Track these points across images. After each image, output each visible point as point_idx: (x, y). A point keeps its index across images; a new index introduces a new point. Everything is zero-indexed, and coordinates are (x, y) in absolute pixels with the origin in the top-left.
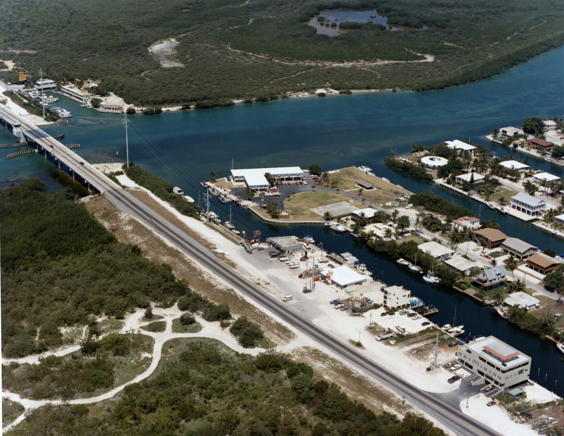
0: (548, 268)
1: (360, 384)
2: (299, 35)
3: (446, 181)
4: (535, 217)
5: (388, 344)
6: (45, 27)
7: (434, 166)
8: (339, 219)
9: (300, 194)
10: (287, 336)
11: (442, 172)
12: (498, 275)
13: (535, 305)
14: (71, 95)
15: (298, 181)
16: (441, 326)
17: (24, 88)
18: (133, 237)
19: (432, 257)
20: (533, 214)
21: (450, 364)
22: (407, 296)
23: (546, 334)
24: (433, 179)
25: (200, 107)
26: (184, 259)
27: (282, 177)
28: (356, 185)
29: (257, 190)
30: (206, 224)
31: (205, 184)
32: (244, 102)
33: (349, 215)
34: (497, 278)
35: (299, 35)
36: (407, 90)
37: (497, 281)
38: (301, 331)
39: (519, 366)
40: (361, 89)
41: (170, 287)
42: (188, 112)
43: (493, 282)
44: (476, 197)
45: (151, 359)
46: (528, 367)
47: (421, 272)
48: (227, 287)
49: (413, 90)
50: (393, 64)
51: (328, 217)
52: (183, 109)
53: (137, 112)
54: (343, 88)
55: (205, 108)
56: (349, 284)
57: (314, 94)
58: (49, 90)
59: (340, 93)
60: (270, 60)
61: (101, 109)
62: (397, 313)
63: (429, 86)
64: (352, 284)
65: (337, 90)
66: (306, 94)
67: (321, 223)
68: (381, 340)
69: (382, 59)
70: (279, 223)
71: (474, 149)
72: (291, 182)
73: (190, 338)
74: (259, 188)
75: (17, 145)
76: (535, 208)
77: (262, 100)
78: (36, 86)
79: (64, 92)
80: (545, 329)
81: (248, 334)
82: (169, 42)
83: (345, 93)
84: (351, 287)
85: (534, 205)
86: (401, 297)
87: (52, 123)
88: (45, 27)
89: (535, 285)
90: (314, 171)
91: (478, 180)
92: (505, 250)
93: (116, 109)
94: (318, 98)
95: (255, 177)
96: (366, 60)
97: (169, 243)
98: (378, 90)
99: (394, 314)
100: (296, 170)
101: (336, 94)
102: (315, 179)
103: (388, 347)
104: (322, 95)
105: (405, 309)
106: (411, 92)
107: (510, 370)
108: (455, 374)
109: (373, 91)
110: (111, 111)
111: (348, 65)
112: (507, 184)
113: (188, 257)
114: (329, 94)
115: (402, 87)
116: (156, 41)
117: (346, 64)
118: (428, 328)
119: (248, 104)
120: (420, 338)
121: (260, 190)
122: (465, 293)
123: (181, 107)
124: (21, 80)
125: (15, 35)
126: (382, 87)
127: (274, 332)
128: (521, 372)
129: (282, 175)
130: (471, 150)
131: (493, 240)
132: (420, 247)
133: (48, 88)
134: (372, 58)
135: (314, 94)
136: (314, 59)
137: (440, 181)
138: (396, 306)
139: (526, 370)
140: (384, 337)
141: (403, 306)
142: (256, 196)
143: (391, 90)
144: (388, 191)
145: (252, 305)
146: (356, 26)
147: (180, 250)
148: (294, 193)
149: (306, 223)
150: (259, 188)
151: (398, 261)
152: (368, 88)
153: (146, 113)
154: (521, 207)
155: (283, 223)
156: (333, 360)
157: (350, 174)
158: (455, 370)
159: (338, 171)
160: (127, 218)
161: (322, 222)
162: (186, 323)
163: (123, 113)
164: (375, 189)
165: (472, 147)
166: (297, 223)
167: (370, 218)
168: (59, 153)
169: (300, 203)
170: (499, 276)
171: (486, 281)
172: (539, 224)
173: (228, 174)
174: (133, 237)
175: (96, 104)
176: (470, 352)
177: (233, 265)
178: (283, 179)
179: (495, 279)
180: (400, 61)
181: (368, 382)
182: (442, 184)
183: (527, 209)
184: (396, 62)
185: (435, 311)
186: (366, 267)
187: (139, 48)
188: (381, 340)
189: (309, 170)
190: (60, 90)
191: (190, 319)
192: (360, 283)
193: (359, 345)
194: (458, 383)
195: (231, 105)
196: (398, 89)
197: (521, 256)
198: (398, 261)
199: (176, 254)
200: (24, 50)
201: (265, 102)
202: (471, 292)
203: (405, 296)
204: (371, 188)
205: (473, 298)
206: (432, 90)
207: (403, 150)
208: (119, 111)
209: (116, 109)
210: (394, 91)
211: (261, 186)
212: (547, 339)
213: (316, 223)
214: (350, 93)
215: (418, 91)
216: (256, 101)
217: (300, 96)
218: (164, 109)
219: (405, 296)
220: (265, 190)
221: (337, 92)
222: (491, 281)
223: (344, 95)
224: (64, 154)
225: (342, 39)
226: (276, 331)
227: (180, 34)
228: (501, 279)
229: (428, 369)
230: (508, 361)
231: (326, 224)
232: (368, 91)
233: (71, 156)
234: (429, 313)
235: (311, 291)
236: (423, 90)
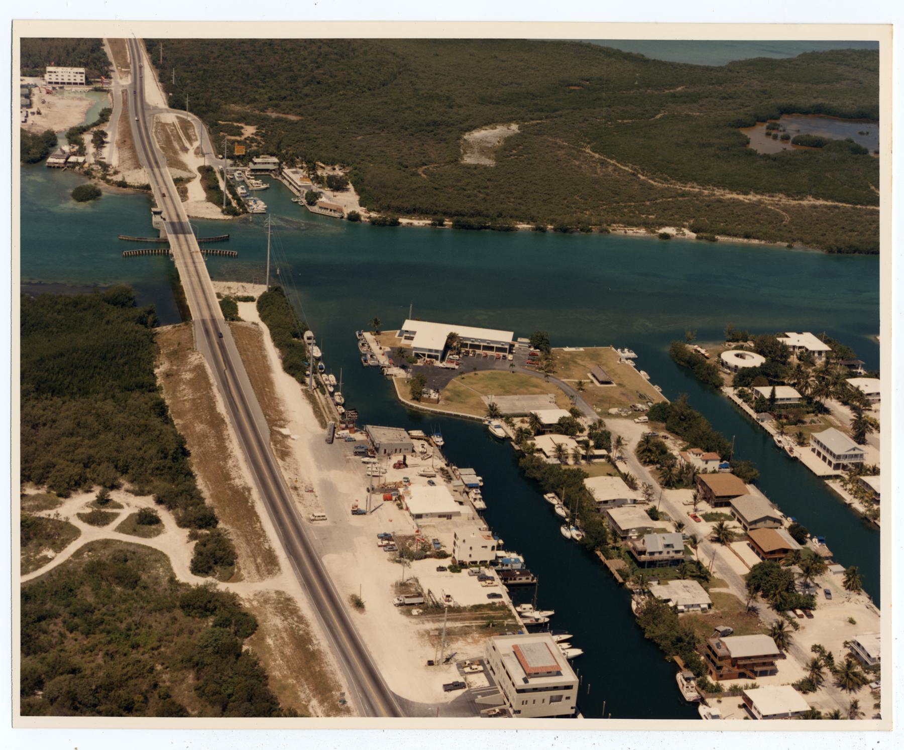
0: (773, 552)
1: (307, 662)
2: (710, 145)
3: (736, 392)
4: (839, 472)
5: (409, 613)
6: (340, 86)
7: (736, 366)
8: (508, 419)
9: (487, 372)
10: (268, 570)
11: (745, 377)
12: (668, 546)
13: (699, 605)
14: (290, 184)
15: (501, 354)
16: (516, 604)
17: (231, 166)
18: (184, 389)
19: (593, 499)
20: (837, 467)
21: (468, 662)
22: (490, 548)
23: (677, 654)
24: (722, 384)
25: (458, 226)
26: (222, 433)
27: (476, 343)
28: (589, 375)
29: (424, 355)
30: (306, 392)
31: (360, 335)
32: (533, 229)
33: (526, 415)
34: (665, 550)
35: (710, 145)
36: (814, 248)
37: (665, 556)
38: (293, 566)
39: (556, 688)
40: (735, 236)
41: (164, 467)
42: (441, 231)
43: (657, 557)
44: (769, 425)
45: (51, 559)
46: (573, 693)
47: (567, 520)
48: (246, 483)
49: (822, 249)
50: (826, 207)
51: (494, 413)
52: (432, 224)
53: (362, 219)
54: (705, 231)
55: (467, 229)
56: (427, 515)
57: (654, 232)
59: (697, 238)
60: (634, 174)
61: (315, 209)
62: (465, 572)
63: (850, 247)
64: (432, 515)
65: (695, 232)
66: (642, 232)
67: (481, 420)
68: (400, 605)
69: (816, 197)
70: (417, 408)
71: (826, 352)
72: (489, 353)
73: (131, 544)
74: (427, 353)
75: (154, 240)
76: (839, 457)
77: (563, 230)
78: (251, 164)
79: (285, 178)
80: (680, 644)
81: (213, 557)
82: (505, 129)
83: (706, 238)
84: (430, 519)
85: (837, 452)
86: (477, 547)
87: (230, 217)
88: (340, 86)
89: (734, 576)
90: (540, 342)
91: (781, 399)
92: (733, 514)
94: (657, 239)
95: (428, 335)
96: (788, 195)
97: (221, 407)
98: (763, 242)
99: (459, 571)
100: (505, 337)
101: (690, 239)
102: (533, 354)
103: (404, 619)
104: (666, 236)
105: (483, 568)
106: (818, 252)
107: (535, 690)
108: (465, 679)
109: (756, 242)
111: (753, 198)
112: (842, 414)
113: (231, 432)
114: (679, 236)
115: (806, 243)
116: (486, 124)
117: (755, 199)
118: (494, 603)
119: (538, 232)
120: (467, 614)
121: (429, 356)
122: (606, 565)
123: (429, 222)
124: (236, 154)
125: (288, 92)
126: (771, 238)
127: (255, 560)
128: (559, 699)
129: (477, 340)
130: (820, 353)
131: (718, 493)
132: (589, 483)
134: (798, 193)
135: (654, 232)
136: (704, 183)
137: (730, 392)
138: (467, 560)
139: (568, 698)
140: (408, 601)
141: (481, 562)
142: (418, 364)
143: (786, 244)
144: (632, 392)
145: (257, 517)
146: (818, 144)
147: (227, 420)
148: (475, 369)
149: (458, 416)
150: (427, 353)
151: (545, 496)
152: (747, 236)
153: (374, 222)
154: (823, 453)
155: (423, 410)
156: (301, 619)
157: (595, 357)
158: (471, 673)
159: (582, 349)
160: (196, 363)
161: (482, 418)
162: (146, 522)
163: (342, 217)
164: (614, 385)
165: (825, 347)
166: (444, 414)
167: (551, 425)
168: (184, 258)
169: (474, 386)
170: (670, 549)
171: (644, 553)
172: (835, 486)
173: (399, 326)
174: (184, 389)
175: (312, 198)
176: (494, 648)
177: (284, 454)
178: (478, 347)
179: (660, 553)
180: (837, 203)
181: (321, 660)
182: (731, 396)
183: (829, 457)
184: (829, 203)
185: (529, 581)
186: (481, 494)
187: (447, 129)
188: (400, 605)
189: (530, 339)
191: (153, 516)
192: (448, 516)
193: (359, 604)
194: (458, 693)
195: (510, 230)
196: (798, 246)
197: (749, 528)
198: (545, 496)
199: (216, 422)
200: (288, 114)
201: (568, 234)
202: (615, 565)
203: (486, 547)
204: (609, 383)
205: (612, 574)
206: (857, 254)
207: (704, 337)
208: (337, 215)
210: (790, 247)
211: (430, 350)
212: (675, 662)
213: (473, 419)
214: (715, 240)
215: (831, 251)
216: (555, 230)
217: (630, 233)
218: (404, 221)
219: (486, 547)
220: (436, 358)
221: (694, 235)
222: (652, 554)
223: (703, 242)
225: (775, 160)
226: (259, 560)
227: (532, 119)
228: (672, 554)
229: (430, 663)
230: (537, 675)
231: (486, 423)
232: (746, 240)
233: (198, 265)
234: (518, 581)
235: (364, 513)
236: (839, 251)
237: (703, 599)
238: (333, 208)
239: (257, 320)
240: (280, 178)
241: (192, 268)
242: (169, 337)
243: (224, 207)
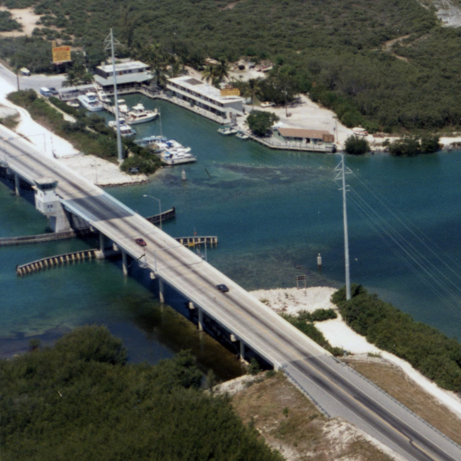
14: (194, 103)
17: (65, 84)
53: (373, 148)
58: (132, 90)
61: (274, 141)
78: (97, 78)
79: (174, 94)
87: (142, 177)
93: (315, 140)
110: (303, 145)
124: (57, 61)
133: (131, 84)
153: (396, 152)
160: (346, 438)
163: (335, 150)
168: (161, 260)
190: (162, 88)
208: (323, 147)
209: (315, 140)
224: (174, 263)
233: (195, 267)
237: (276, 428)
238: (315, 136)
239: (373, 349)
240: (163, 96)
241: (192, 277)
242: (254, 402)
243: (121, 161)
